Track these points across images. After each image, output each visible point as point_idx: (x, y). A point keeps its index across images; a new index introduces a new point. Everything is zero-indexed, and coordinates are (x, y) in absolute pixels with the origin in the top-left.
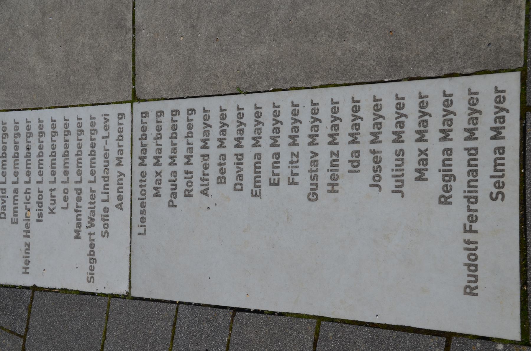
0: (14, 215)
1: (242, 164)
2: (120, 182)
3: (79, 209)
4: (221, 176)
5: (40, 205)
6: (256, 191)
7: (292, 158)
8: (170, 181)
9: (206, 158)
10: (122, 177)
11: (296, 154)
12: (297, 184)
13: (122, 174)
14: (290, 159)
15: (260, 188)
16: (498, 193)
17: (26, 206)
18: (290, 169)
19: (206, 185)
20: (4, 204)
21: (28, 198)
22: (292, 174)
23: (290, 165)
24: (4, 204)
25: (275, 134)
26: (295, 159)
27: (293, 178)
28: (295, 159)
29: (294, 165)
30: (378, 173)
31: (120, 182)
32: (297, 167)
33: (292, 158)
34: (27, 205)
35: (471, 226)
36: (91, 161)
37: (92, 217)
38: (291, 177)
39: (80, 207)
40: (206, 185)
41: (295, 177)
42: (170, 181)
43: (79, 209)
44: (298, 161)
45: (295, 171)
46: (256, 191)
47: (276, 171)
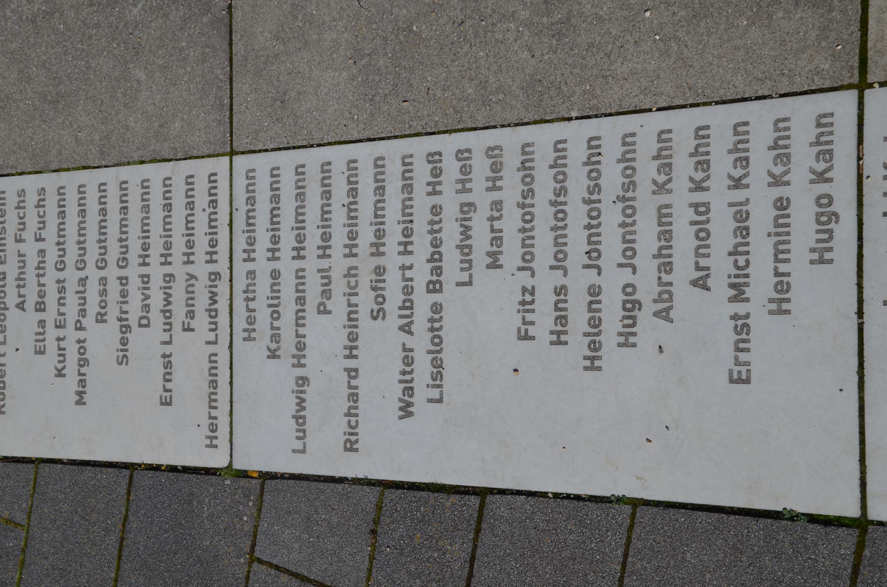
0: (166, 390)
1: (148, 289)
2: (190, 289)
3: (124, 316)
4: (40, 300)
5: (168, 314)
6: (740, 372)
7: (524, 295)
8: (77, 292)
9: (124, 281)
10: (193, 281)
11: (530, 288)
12: (533, 338)
13: (192, 277)
14: (521, 298)
15: (748, 367)
16: (379, 311)
17: (121, 308)
18: (521, 314)
19: (407, 317)
20: (146, 302)
21: (353, 284)
22: (525, 322)
23: (521, 307)
24: (146, 302)
25: (495, 249)
26: (528, 298)
27: (526, 330)
28: (528, 298)
29: (527, 307)
30: (104, 298)
31: (190, 289)
32: (533, 311)
33: (524, 295)
34: (123, 306)
35: (189, 323)
36: (322, 210)
37: (406, 398)
38: (523, 328)
39: (126, 312)
40: (407, 317)
41: (530, 327)
42: (77, 292)
43: (124, 316)
44: (533, 302)
45: (529, 317)
46: (740, 372)
47: (703, 262)
